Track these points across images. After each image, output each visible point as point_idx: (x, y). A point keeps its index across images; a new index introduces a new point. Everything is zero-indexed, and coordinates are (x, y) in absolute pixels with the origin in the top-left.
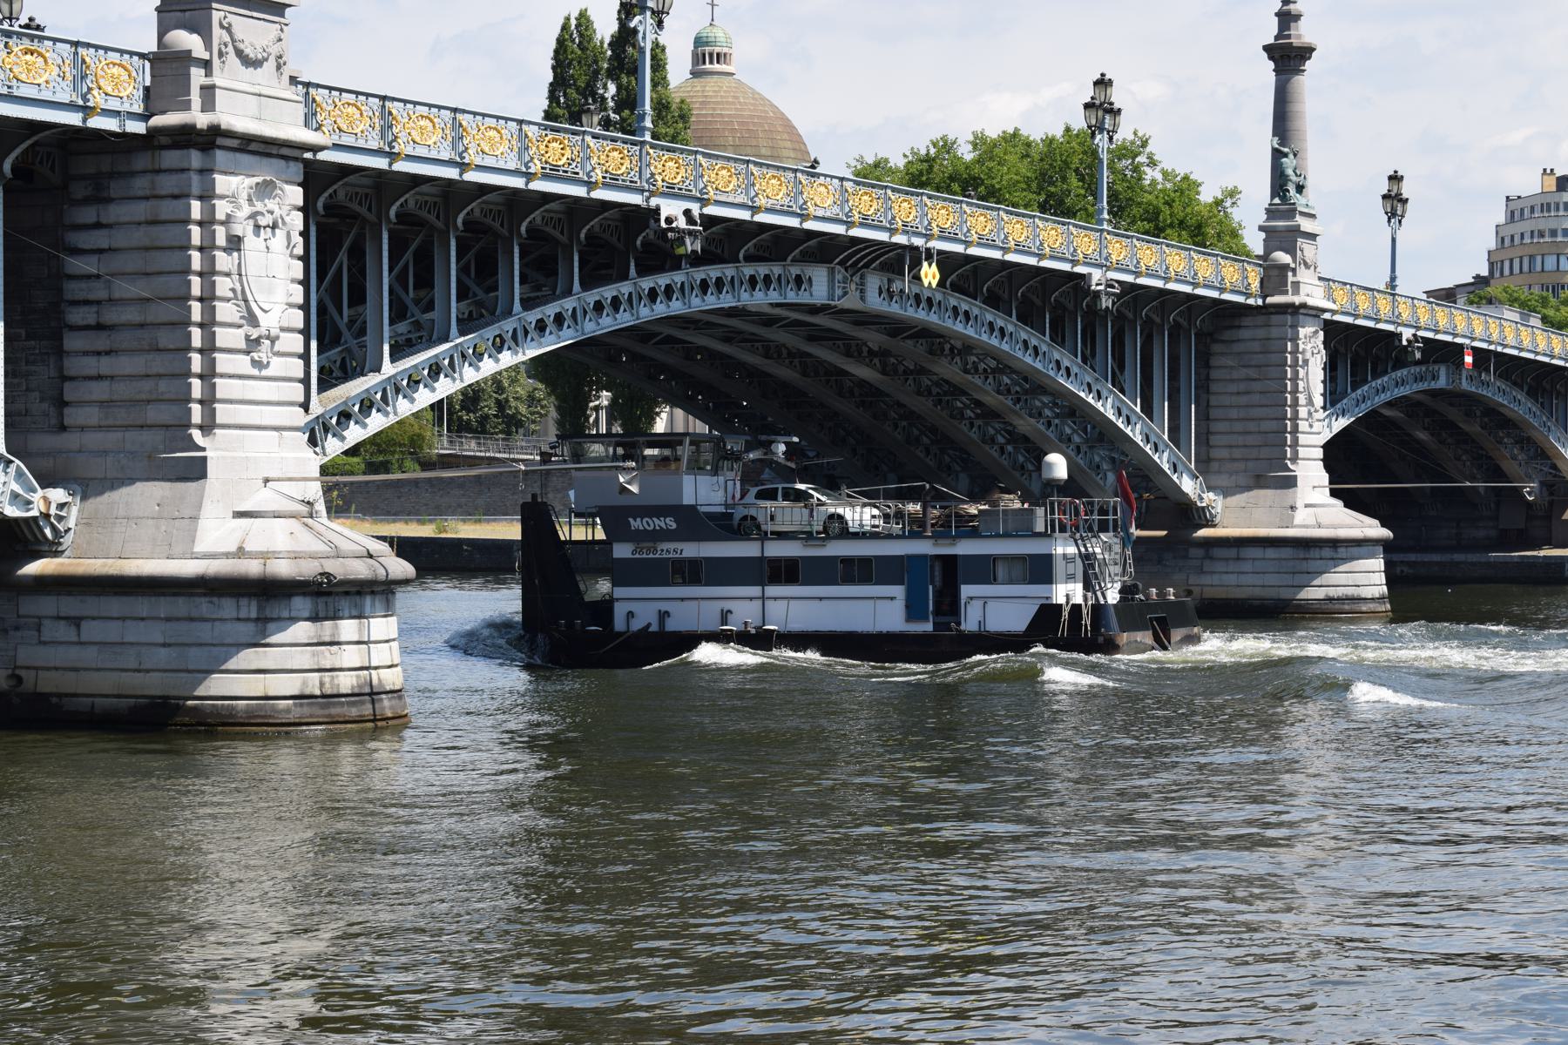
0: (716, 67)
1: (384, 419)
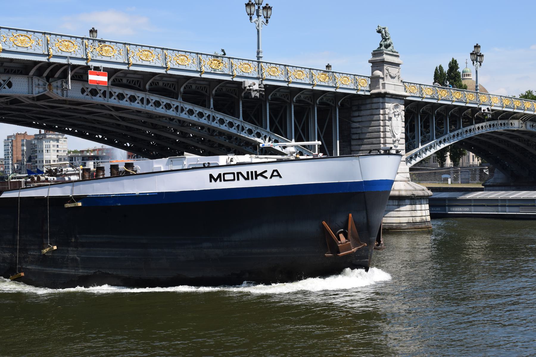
1: (420, 159)
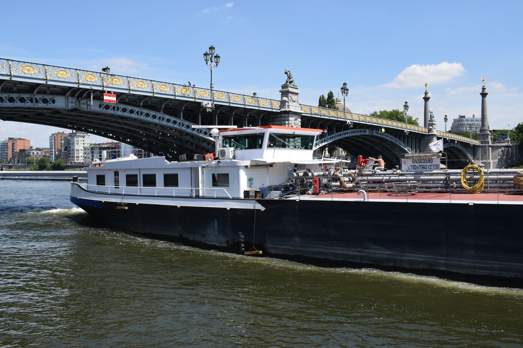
0: (339, 102)
